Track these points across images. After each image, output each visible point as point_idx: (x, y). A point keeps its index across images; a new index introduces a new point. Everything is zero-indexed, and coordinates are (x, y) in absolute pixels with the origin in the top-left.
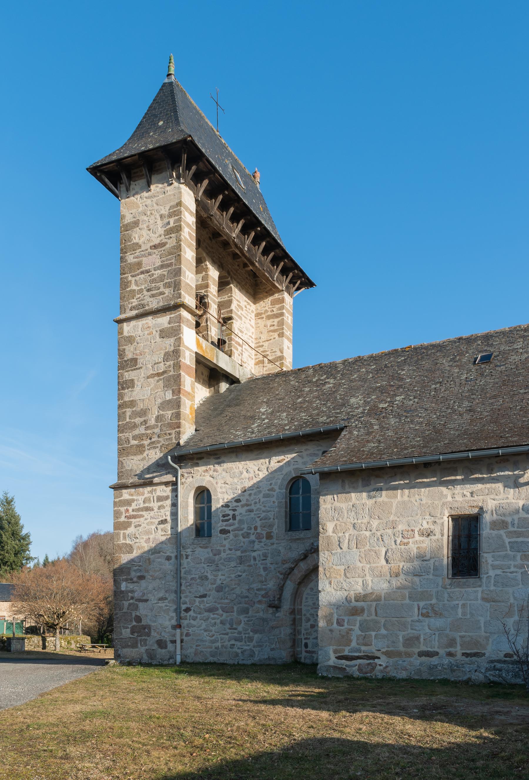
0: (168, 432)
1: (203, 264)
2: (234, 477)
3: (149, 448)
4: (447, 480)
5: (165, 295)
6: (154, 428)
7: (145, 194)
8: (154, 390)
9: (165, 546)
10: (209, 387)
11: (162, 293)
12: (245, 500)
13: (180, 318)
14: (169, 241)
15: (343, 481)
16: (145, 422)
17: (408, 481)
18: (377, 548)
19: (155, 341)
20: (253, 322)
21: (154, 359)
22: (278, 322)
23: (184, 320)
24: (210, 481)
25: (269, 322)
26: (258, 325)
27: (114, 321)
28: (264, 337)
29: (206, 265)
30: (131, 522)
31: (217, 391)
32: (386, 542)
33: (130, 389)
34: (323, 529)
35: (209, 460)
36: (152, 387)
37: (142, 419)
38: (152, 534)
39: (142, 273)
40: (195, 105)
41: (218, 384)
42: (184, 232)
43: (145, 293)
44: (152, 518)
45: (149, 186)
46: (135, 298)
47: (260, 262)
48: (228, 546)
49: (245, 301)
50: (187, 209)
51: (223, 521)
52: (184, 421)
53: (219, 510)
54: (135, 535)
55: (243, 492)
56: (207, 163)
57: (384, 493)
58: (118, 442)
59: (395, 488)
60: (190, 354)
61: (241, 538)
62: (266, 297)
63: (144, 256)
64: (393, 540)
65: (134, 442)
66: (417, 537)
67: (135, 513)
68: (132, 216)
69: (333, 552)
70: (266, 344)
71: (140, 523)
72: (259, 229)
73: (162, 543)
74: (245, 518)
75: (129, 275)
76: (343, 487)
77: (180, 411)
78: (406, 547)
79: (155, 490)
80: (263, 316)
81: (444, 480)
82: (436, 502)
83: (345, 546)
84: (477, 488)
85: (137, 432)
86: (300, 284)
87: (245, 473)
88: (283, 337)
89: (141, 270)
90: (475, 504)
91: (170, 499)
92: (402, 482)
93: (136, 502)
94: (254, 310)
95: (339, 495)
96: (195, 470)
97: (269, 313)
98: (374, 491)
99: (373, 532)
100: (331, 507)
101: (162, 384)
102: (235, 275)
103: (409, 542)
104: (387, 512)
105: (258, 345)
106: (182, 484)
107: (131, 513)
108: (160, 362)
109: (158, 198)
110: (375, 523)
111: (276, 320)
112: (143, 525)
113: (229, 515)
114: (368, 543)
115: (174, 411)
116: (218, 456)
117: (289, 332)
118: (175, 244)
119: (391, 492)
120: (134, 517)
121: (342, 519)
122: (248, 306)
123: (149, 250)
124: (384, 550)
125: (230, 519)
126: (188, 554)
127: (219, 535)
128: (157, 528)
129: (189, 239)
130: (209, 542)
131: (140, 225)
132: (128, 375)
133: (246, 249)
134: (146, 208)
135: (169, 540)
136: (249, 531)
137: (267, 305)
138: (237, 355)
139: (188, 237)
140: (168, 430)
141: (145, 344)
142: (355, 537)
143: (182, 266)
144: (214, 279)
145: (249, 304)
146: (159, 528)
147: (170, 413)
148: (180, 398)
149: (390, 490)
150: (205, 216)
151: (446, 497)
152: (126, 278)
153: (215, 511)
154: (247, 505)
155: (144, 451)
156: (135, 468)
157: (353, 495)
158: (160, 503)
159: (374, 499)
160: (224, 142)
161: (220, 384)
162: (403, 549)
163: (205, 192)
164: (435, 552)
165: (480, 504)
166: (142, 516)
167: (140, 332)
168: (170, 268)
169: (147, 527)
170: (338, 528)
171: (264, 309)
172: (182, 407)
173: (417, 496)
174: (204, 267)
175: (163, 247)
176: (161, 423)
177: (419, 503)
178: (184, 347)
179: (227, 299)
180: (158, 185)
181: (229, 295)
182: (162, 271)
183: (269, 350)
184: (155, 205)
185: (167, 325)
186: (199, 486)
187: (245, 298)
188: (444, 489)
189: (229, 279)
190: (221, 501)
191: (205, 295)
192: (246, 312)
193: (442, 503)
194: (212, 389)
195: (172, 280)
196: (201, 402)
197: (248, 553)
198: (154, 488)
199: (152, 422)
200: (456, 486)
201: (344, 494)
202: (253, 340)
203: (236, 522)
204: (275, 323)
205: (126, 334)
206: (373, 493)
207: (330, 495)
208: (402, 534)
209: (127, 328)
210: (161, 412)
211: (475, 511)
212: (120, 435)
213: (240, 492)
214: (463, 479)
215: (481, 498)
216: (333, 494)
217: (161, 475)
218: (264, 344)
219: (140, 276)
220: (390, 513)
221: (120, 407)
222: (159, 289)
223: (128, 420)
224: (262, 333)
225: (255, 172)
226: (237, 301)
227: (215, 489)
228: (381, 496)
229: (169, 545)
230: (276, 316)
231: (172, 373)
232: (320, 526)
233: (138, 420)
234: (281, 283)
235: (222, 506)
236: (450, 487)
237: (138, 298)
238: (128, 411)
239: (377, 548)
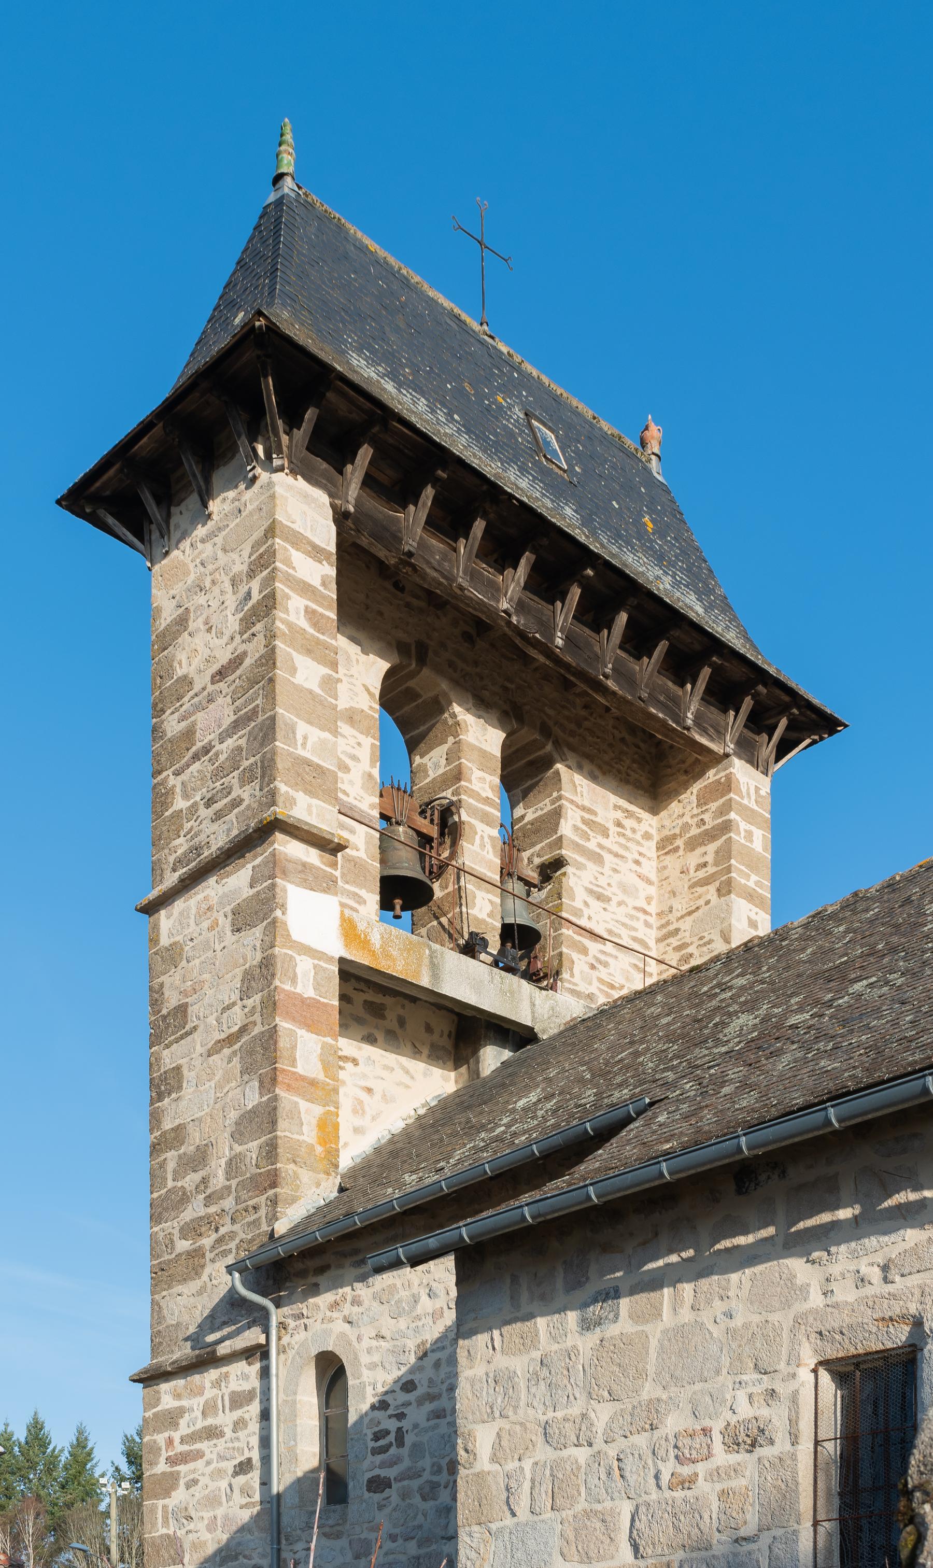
0: (251, 1203)
1: (446, 715)
2: (400, 1315)
3: (212, 1255)
4: (807, 1230)
5: (242, 807)
6: (222, 1198)
7: (200, 531)
8: (222, 1088)
9: (249, 1537)
10: (456, 1067)
11: (237, 802)
12: (426, 1383)
13: (275, 863)
14: (249, 647)
15: (515, 1279)
16: (205, 1181)
17: (690, 1253)
18: (608, 1504)
19: (222, 945)
20: (649, 868)
21: (221, 998)
22: (717, 852)
23: (290, 866)
24: (343, 1335)
25: (693, 859)
26: (666, 873)
27: (136, 910)
28: (680, 905)
29: (454, 716)
30: (178, 1473)
31: (475, 1073)
32: (632, 1479)
33: (174, 1095)
34: (467, 1451)
35: (340, 1272)
36: (217, 1078)
37: (196, 1177)
38: (220, 1504)
39: (196, 757)
40: (382, 253)
41: (475, 1052)
42: (287, 611)
43: (204, 812)
44: (221, 1458)
45: (205, 506)
46: (182, 834)
47: (620, 673)
48: (387, 1529)
49: (616, 807)
50: (297, 540)
51: (376, 1452)
52: (292, 1166)
53: (366, 1420)
54: (186, 1509)
55: (421, 1358)
56: (352, 393)
57: (624, 1303)
58: (152, 1249)
59: (655, 1283)
60: (315, 966)
61: (417, 1500)
62: (686, 786)
63: (199, 708)
64: (652, 1472)
65: (183, 1245)
66: (721, 1457)
67: (186, 1448)
68: (174, 602)
69: (493, 1527)
70: (686, 925)
71: (196, 1476)
72: (590, 572)
73: (242, 1529)
74: (425, 1438)
75: (170, 772)
76: (514, 1299)
77: (276, 1137)
78: (688, 1493)
79: (227, 1375)
80: (679, 842)
81: (798, 1232)
82: (775, 1318)
83: (522, 1504)
84: (901, 1247)
85: (188, 1215)
86: (788, 728)
87: (424, 1298)
88: (729, 892)
89: (194, 749)
90: (896, 1309)
91: (258, 1400)
92: (674, 1258)
93: (187, 1414)
94: (653, 832)
95: (505, 1329)
96: (310, 1307)
97: (694, 831)
98: (595, 1301)
99: (596, 1448)
100: (487, 1374)
101: (239, 1066)
102: (572, 734)
103: (696, 1475)
104: (632, 1372)
105: (665, 931)
106: (282, 1350)
107: (180, 1448)
108: (234, 1004)
109: (227, 530)
110: (602, 1414)
111: (712, 848)
112: (203, 1481)
113: (388, 1433)
114: (583, 1490)
115: (264, 1139)
116: (360, 1257)
117: (754, 878)
118: (262, 651)
119: (642, 1298)
120: (184, 1458)
121: (515, 1413)
122: (629, 823)
123: (210, 688)
124: (626, 1509)
125: (391, 1444)
126: (297, 1556)
127: (367, 1495)
128: (230, 1485)
129: (311, 631)
130: (344, 1517)
131: (190, 623)
132: (169, 1058)
133: (559, 642)
134: (202, 569)
135: (256, 1518)
136: (435, 1478)
137: (689, 808)
138: (586, 968)
139: (303, 623)
140: (251, 1198)
141: (202, 958)
142: (548, 1472)
143: (279, 710)
144: (484, 754)
145: (629, 814)
146: (234, 1487)
147: (254, 1145)
148: (275, 1098)
149: (642, 1291)
150: (393, 561)
151: (804, 1291)
152: (163, 783)
153: (355, 1424)
154: (432, 1398)
155: (203, 1266)
156: (186, 1318)
157: (541, 1322)
158: (237, 1414)
159: (598, 1329)
160: (504, 349)
161: (482, 1051)
162: (679, 1502)
163: (369, 482)
164: (773, 1503)
165: (913, 1308)
166: (199, 1455)
167: (192, 929)
168: (253, 724)
169: (213, 1485)
170: (505, 1443)
171: (680, 822)
172: (282, 1124)
173: (717, 1303)
174: (450, 721)
175: (237, 667)
176: (237, 1180)
177: (723, 1326)
178: (290, 948)
179: (549, 808)
180: (225, 494)
181: (555, 794)
182: (235, 737)
183: (695, 939)
184: (220, 554)
185: (248, 892)
186: (323, 1352)
187: (613, 799)
188: (796, 1265)
189: (549, 747)
190: (369, 1391)
191: (452, 803)
192: (622, 840)
193: (791, 1317)
194: (463, 1069)
195: (257, 757)
196: (422, 1112)
197: (434, 1547)
198: (224, 1369)
199: (219, 1180)
200: (833, 1249)
201: (519, 1324)
202: (652, 920)
203: (405, 1451)
204: (710, 858)
205: (164, 941)
206: (595, 1310)
207: (482, 1332)
208: (676, 1447)
209: (166, 920)
210: (238, 1148)
211: (900, 1335)
212: (155, 1229)
213: (412, 1359)
214: (856, 1217)
215: (915, 1280)
216: (490, 1329)
217: (238, 1332)
218: (682, 925)
219: (191, 768)
220: (642, 1374)
221: (155, 1149)
222: (229, 793)
223: (170, 1184)
224: (674, 894)
225: (647, 428)
226: (584, 808)
227: (356, 1355)
228: (617, 1316)
229: (256, 1533)
230: (710, 836)
231: (258, 1029)
232: (459, 1441)
233: (190, 1180)
234: (719, 734)
235: (373, 1407)
236: (815, 1255)
237: (188, 833)
238: (171, 1157)
239: (608, 1504)
